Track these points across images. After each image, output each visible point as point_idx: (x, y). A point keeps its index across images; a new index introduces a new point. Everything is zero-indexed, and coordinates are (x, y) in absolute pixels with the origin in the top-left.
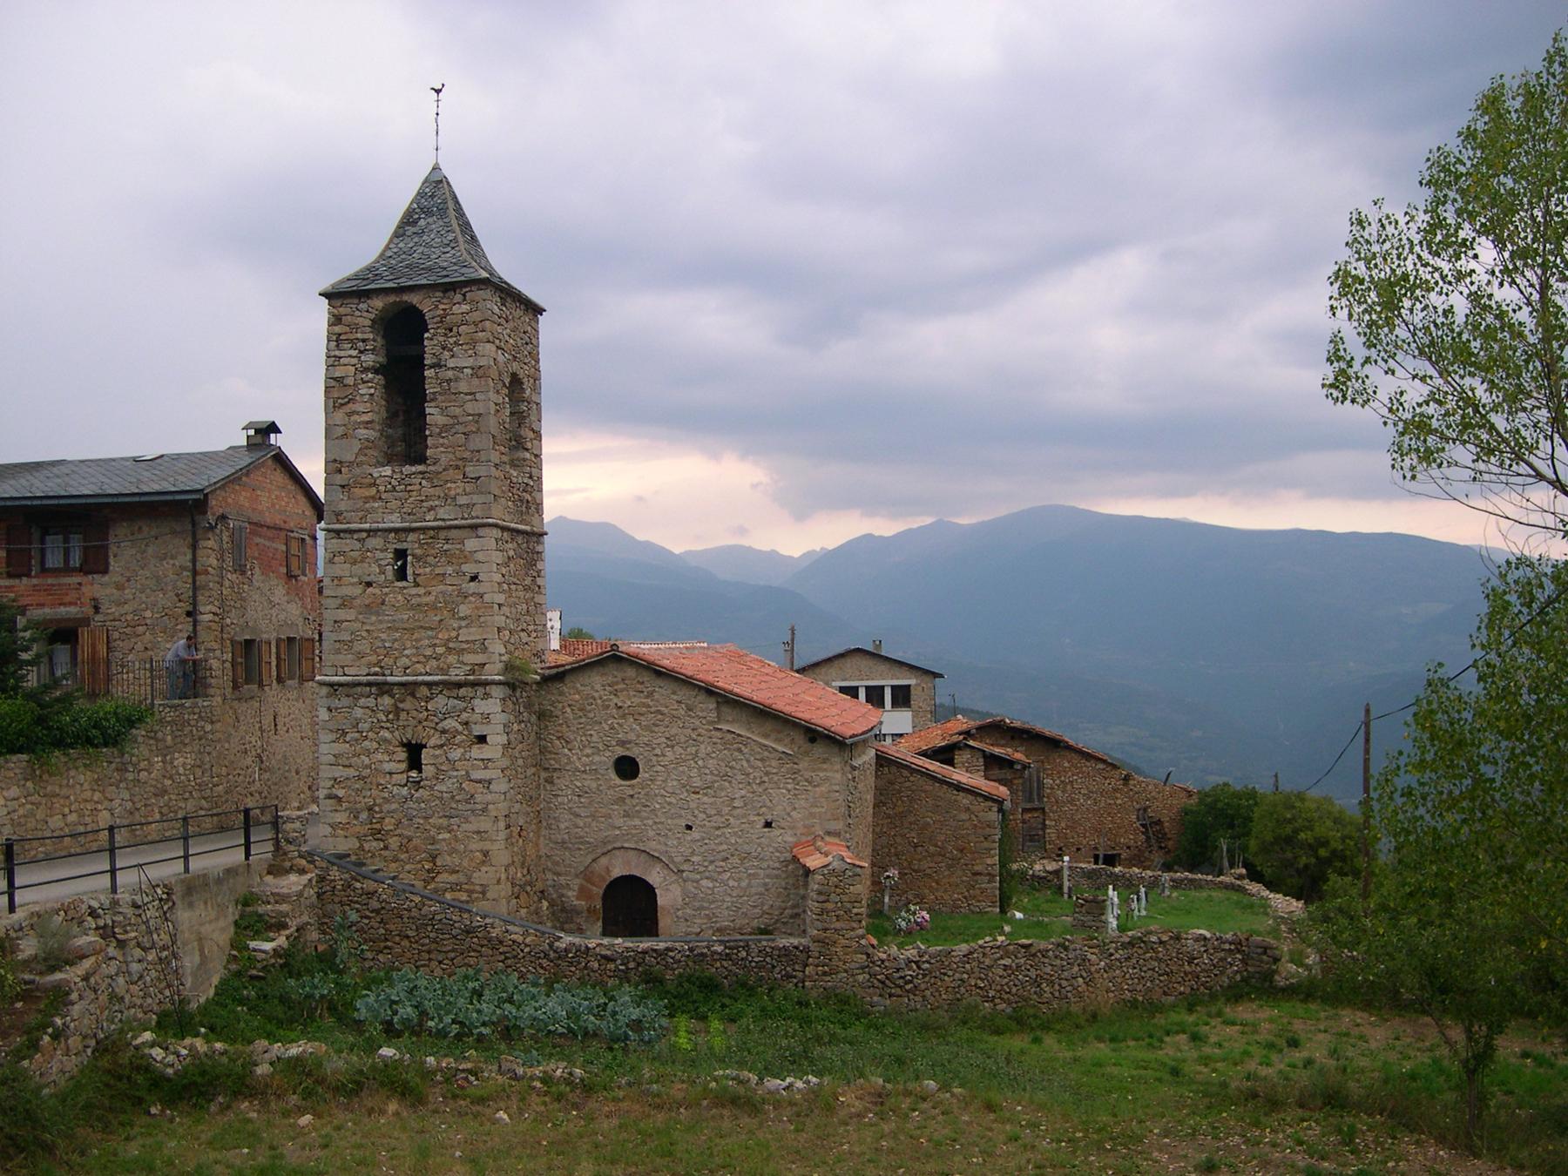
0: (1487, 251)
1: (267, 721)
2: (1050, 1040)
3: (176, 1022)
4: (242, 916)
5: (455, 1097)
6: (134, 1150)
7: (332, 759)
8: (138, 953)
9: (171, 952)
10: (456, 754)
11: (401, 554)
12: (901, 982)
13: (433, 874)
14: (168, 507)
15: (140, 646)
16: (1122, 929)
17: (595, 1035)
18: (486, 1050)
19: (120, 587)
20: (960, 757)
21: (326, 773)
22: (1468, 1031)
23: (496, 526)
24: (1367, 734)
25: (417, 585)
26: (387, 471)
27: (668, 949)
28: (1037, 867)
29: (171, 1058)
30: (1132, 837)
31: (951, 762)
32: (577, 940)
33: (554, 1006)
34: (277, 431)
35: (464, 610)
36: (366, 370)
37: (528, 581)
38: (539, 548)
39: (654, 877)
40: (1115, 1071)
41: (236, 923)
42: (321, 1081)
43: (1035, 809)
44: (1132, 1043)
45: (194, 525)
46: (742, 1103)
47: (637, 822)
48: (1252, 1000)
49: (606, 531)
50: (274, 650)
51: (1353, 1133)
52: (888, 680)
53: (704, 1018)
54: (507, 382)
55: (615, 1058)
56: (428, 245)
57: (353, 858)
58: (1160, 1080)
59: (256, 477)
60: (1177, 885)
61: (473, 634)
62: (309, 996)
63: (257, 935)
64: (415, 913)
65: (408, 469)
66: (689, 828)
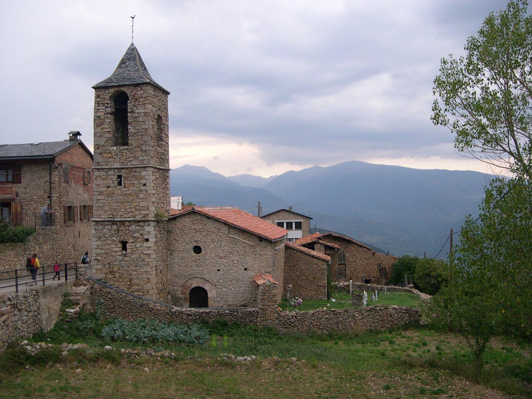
0: (487, 73)
1: (77, 234)
2: (341, 343)
3: (39, 336)
4: (64, 300)
5: (131, 363)
6: (19, 381)
7: (96, 247)
8: (26, 313)
9: (38, 312)
10: (138, 245)
11: (120, 177)
12: (290, 323)
13: (131, 285)
14: (42, 161)
15: (32, 208)
16: (367, 305)
17: (184, 341)
18: (145, 346)
19: (25, 188)
20: (316, 247)
21: (94, 251)
22: (477, 341)
23: (152, 167)
24: (451, 239)
25: (125, 187)
26: (115, 148)
27: (210, 312)
28: (341, 284)
29: (34, 349)
30: (375, 274)
31: (313, 249)
32: (179, 309)
33: (170, 331)
34: (80, 135)
35: (141, 196)
36: (108, 114)
37: (164, 186)
38: (168, 175)
39: (207, 287)
40: (362, 354)
41: (62, 303)
42: (84, 357)
43: (343, 264)
44: (369, 344)
45: (50, 166)
46: (229, 365)
47: (201, 268)
48: (412, 330)
49: (202, 169)
50: (79, 209)
51: (437, 376)
52: (294, 220)
53: (222, 335)
54: (156, 117)
55: (189, 349)
56: (129, 71)
57: (104, 280)
58: (377, 357)
59: (73, 151)
60: (389, 290)
61: (144, 204)
62: (86, 328)
63: (69, 307)
64: (123, 299)
65: (122, 147)
66: (219, 270)
